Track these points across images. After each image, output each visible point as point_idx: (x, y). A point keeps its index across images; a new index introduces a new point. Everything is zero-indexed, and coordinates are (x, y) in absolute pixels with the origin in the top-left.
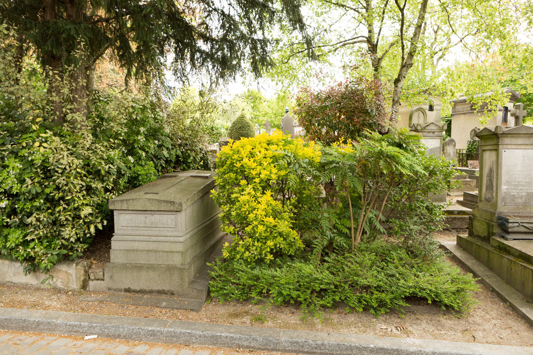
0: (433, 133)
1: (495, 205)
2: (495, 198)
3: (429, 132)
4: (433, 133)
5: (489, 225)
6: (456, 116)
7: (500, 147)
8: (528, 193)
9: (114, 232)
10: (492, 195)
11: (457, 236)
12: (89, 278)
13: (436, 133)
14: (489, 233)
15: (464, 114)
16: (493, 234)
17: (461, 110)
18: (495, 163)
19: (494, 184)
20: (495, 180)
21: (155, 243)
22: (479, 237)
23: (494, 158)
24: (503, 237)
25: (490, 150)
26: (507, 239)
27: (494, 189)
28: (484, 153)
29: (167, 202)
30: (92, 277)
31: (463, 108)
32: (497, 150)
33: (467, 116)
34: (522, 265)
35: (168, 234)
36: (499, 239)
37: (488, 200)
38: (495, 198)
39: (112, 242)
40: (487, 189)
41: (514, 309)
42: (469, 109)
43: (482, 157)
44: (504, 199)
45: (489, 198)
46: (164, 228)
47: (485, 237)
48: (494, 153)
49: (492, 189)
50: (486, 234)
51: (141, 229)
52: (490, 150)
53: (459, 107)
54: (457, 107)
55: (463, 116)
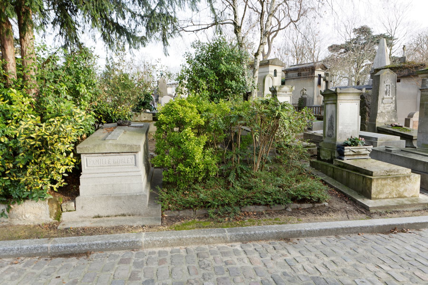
0: (286, 92)
1: (335, 139)
2: (335, 134)
3: (283, 92)
4: (286, 92)
5: (332, 152)
6: (288, 80)
7: (338, 101)
8: (353, 131)
9: (81, 172)
10: (333, 133)
11: (310, 161)
12: (62, 210)
13: (288, 93)
14: (332, 157)
15: (294, 79)
16: (335, 158)
17: (291, 76)
18: (334, 112)
19: (334, 126)
20: (334, 123)
21: (119, 178)
22: (324, 160)
23: (334, 109)
24: (341, 159)
25: (330, 103)
26: (343, 160)
27: (334, 129)
28: (327, 105)
29: (121, 145)
30: (64, 210)
31: (293, 75)
32: (336, 104)
33: (295, 80)
34: (356, 174)
35: (129, 170)
36: (339, 160)
37: (330, 136)
38: (335, 134)
39: (81, 180)
40: (329, 129)
41: (355, 202)
42: (297, 75)
43: (326, 108)
44: (340, 134)
45: (330, 135)
46: (125, 165)
47: (329, 160)
48: (334, 106)
49: (333, 129)
50: (330, 158)
51: (105, 168)
52: (330, 103)
53: (290, 74)
54: (289, 74)
55: (292, 81)
